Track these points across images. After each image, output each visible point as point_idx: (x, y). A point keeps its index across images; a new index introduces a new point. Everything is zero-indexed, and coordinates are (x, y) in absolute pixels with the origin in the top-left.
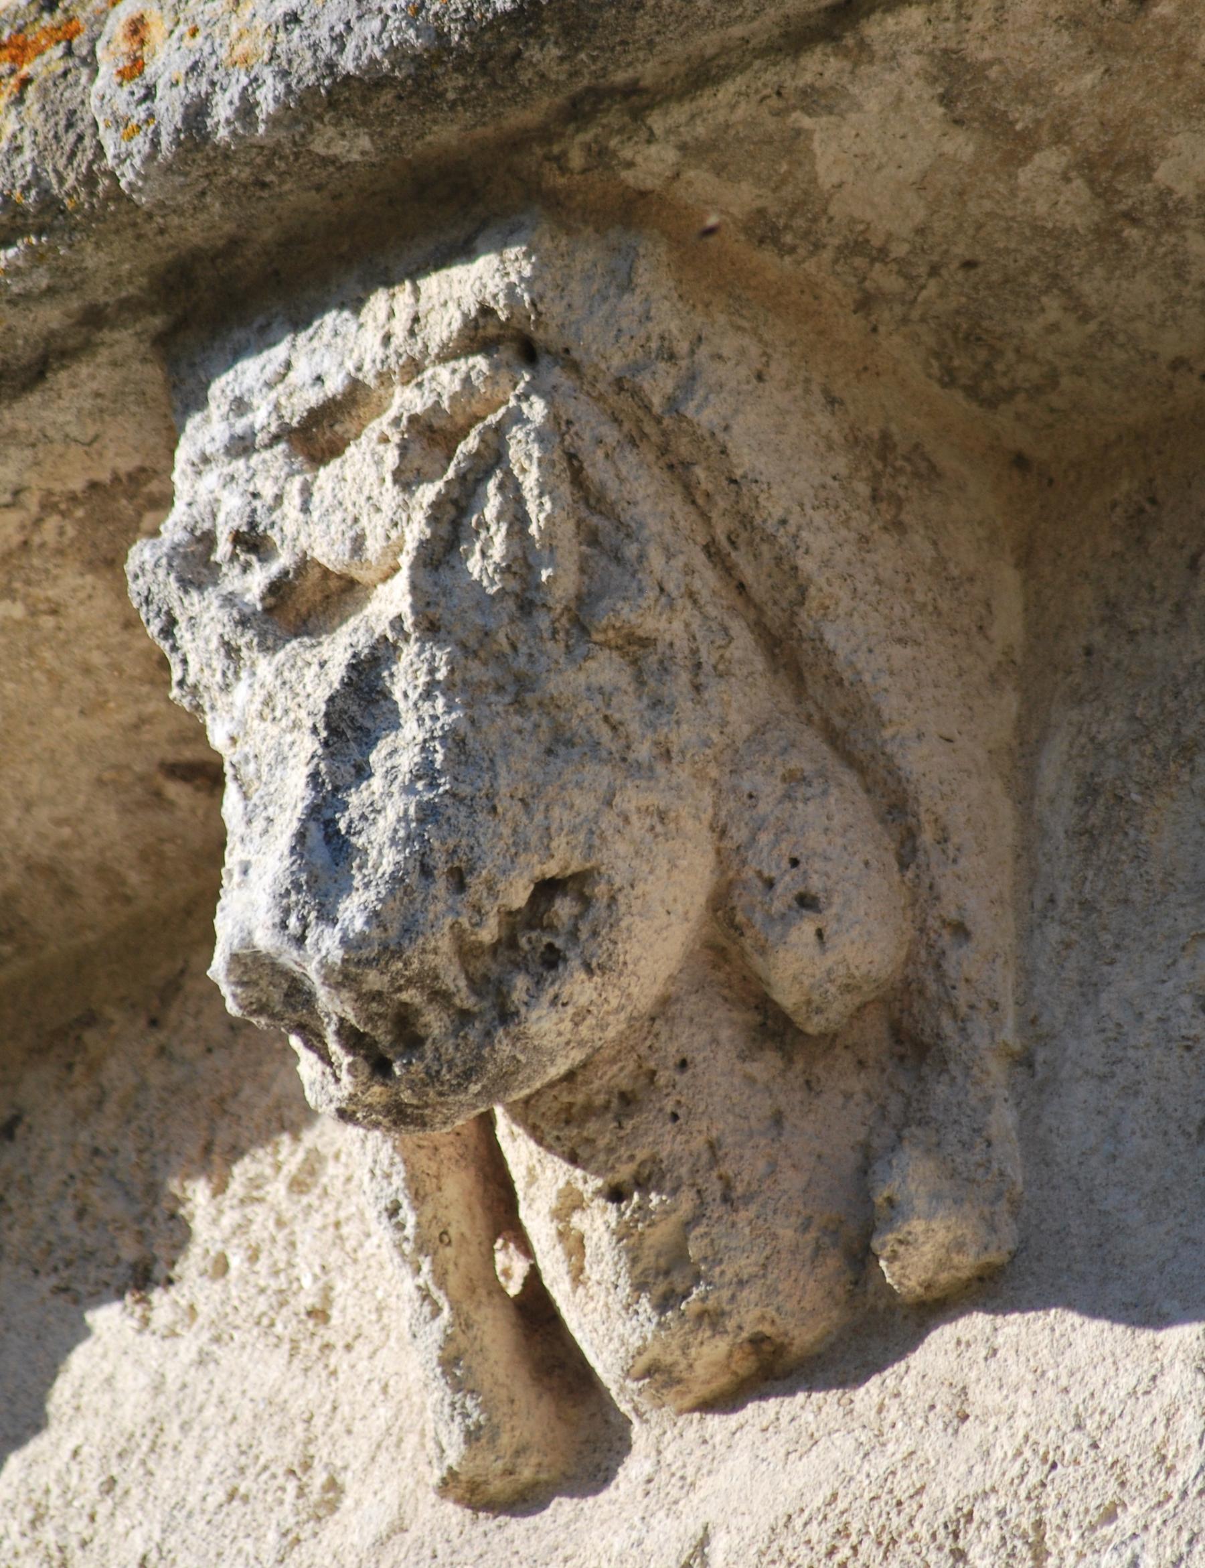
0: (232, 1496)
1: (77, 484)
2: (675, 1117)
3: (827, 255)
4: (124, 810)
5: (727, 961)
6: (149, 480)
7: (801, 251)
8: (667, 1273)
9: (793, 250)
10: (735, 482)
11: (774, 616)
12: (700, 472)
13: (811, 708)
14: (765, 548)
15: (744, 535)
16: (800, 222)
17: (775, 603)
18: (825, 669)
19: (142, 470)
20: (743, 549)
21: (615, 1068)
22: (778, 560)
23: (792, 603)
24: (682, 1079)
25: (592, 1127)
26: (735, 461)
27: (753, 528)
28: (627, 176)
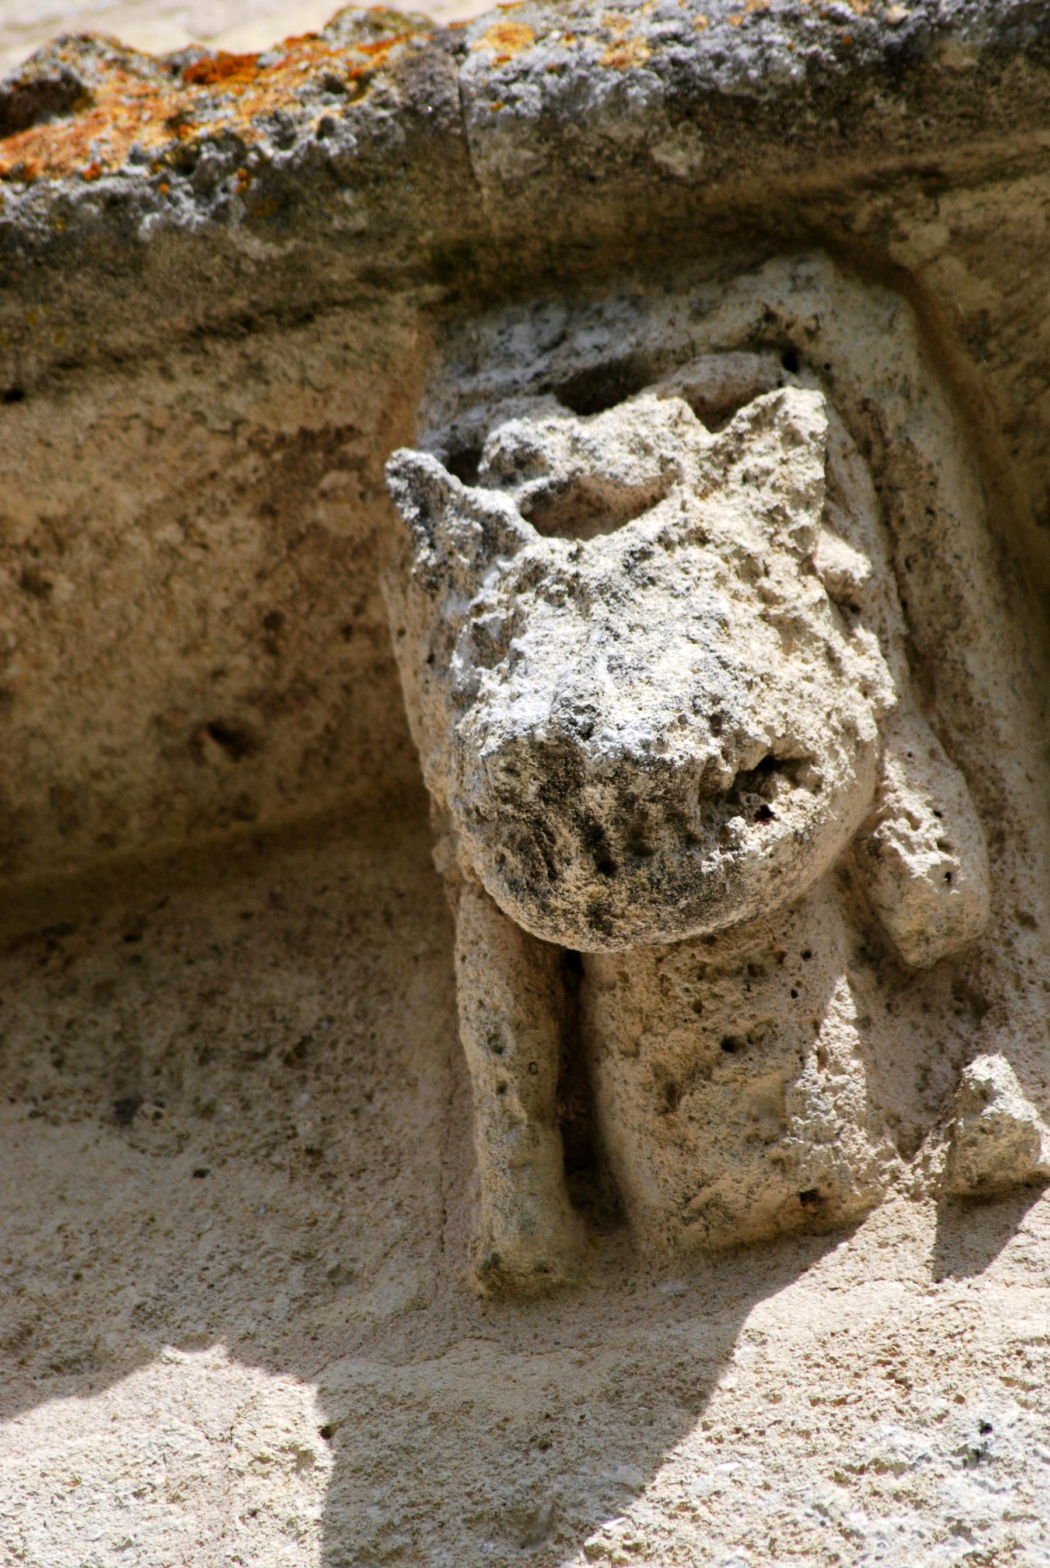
0: (234, 1268)
1: (290, 429)
2: (794, 994)
3: (1014, 370)
4: (166, 754)
5: (849, 887)
6: (351, 439)
7: (997, 361)
8: (756, 1120)
9: (989, 357)
10: (930, 512)
11: (926, 635)
12: (904, 497)
13: (935, 719)
14: (937, 575)
15: (922, 561)
16: (1011, 331)
17: (930, 624)
18: (957, 688)
19: (350, 428)
20: (917, 572)
21: (752, 943)
22: (946, 588)
23: (945, 627)
24: (806, 966)
25: (723, 985)
26: (940, 494)
27: (933, 557)
28: (895, 248)
